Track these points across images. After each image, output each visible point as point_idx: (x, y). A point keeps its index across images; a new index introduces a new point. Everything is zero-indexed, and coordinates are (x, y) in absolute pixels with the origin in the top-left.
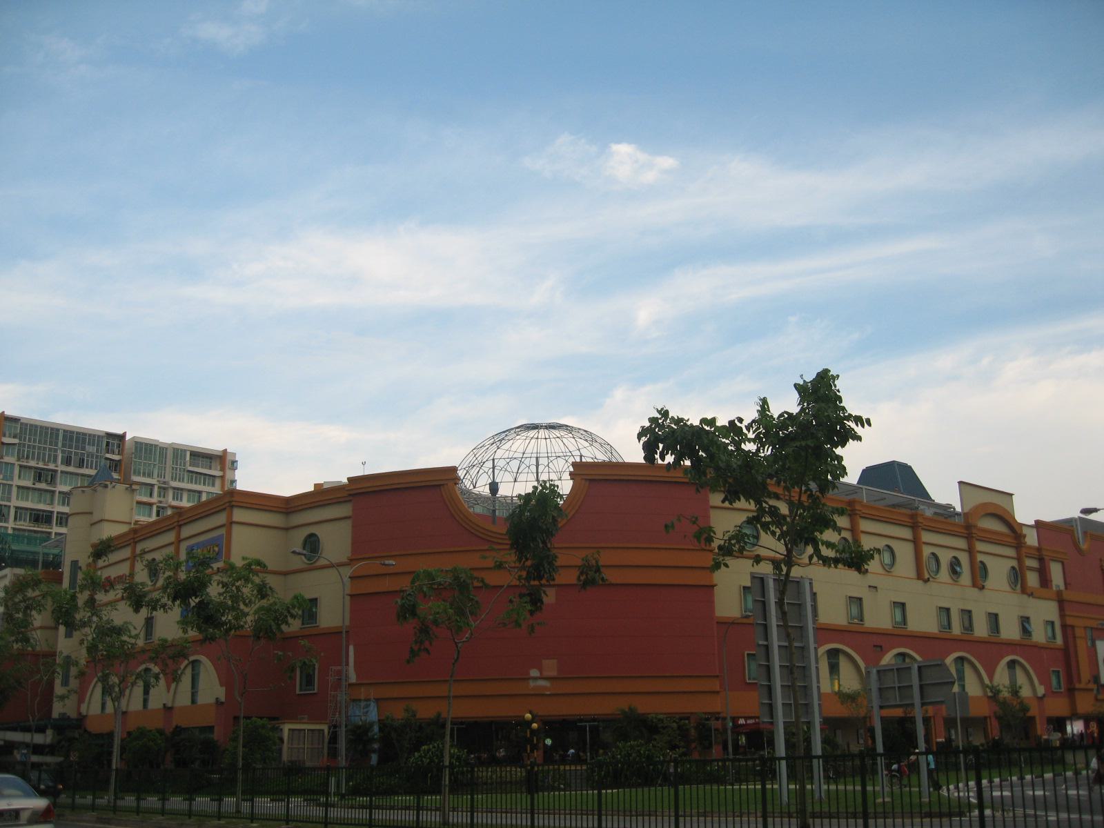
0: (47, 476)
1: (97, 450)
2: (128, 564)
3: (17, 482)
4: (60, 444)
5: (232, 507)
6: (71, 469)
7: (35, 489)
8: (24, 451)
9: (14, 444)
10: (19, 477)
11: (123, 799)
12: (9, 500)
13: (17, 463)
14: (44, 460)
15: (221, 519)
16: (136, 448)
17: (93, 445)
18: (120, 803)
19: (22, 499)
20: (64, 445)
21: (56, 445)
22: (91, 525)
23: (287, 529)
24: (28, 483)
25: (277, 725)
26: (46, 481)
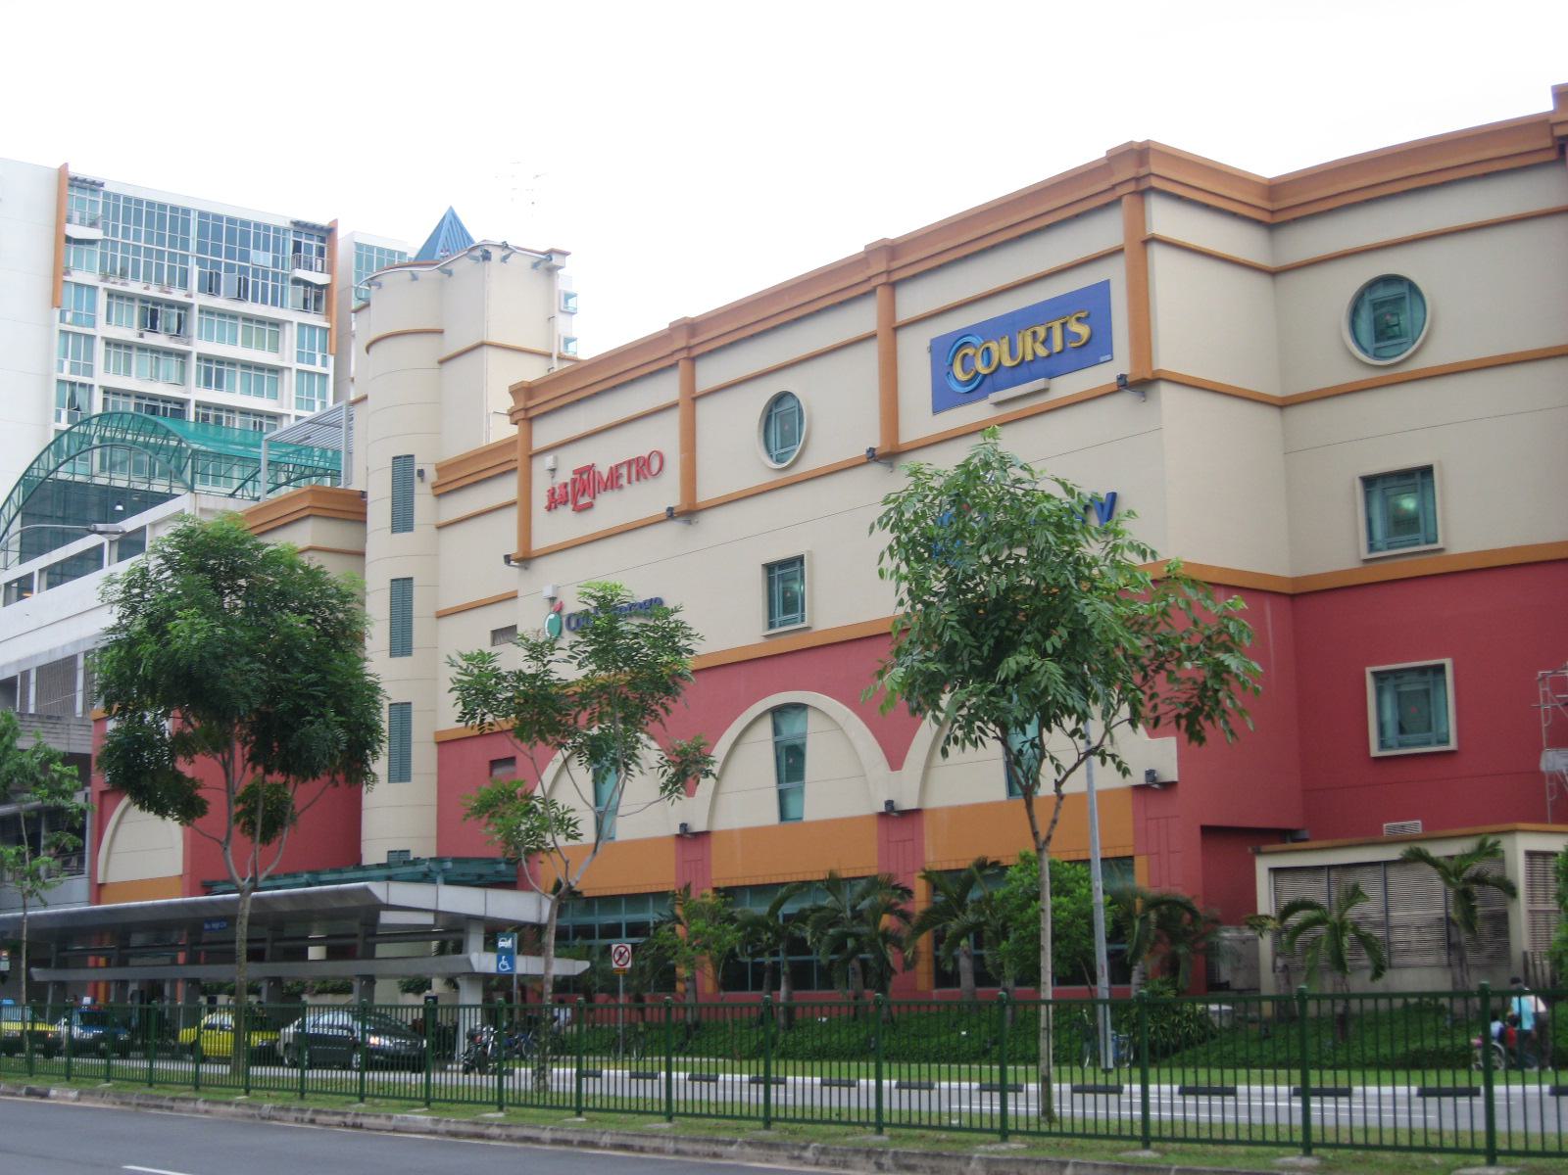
0: (169, 317)
1: (276, 260)
2: (673, 419)
3: (103, 330)
4: (193, 245)
5: (1142, 194)
6: (220, 302)
7: (143, 348)
8: (114, 258)
9: (92, 242)
10: (108, 319)
11: (598, 1075)
12: (89, 371)
13: (102, 285)
14: (159, 280)
15: (1106, 231)
16: (359, 257)
17: (266, 249)
18: (590, 1086)
19: (117, 372)
20: (202, 248)
21: (185, 245)
22: (442, 362)
23: (1273, 273)
24: (129, 334)
25: (1491, 840)
26: (167, 330)
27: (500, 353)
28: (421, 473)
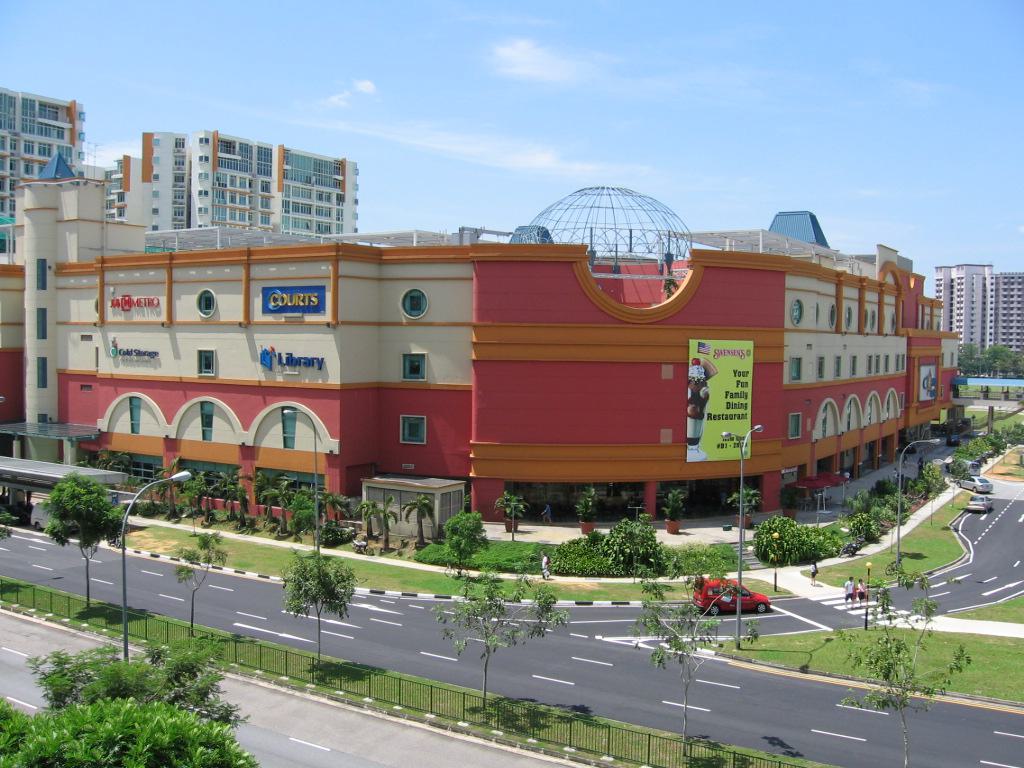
27: (92, 218)
28: (50, 267)
